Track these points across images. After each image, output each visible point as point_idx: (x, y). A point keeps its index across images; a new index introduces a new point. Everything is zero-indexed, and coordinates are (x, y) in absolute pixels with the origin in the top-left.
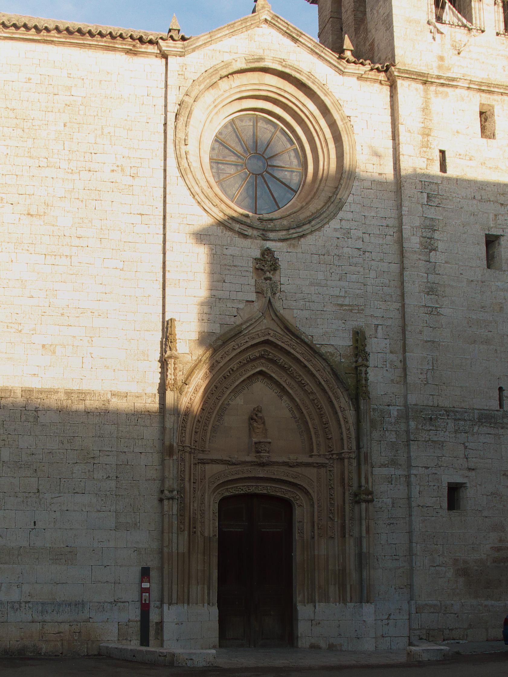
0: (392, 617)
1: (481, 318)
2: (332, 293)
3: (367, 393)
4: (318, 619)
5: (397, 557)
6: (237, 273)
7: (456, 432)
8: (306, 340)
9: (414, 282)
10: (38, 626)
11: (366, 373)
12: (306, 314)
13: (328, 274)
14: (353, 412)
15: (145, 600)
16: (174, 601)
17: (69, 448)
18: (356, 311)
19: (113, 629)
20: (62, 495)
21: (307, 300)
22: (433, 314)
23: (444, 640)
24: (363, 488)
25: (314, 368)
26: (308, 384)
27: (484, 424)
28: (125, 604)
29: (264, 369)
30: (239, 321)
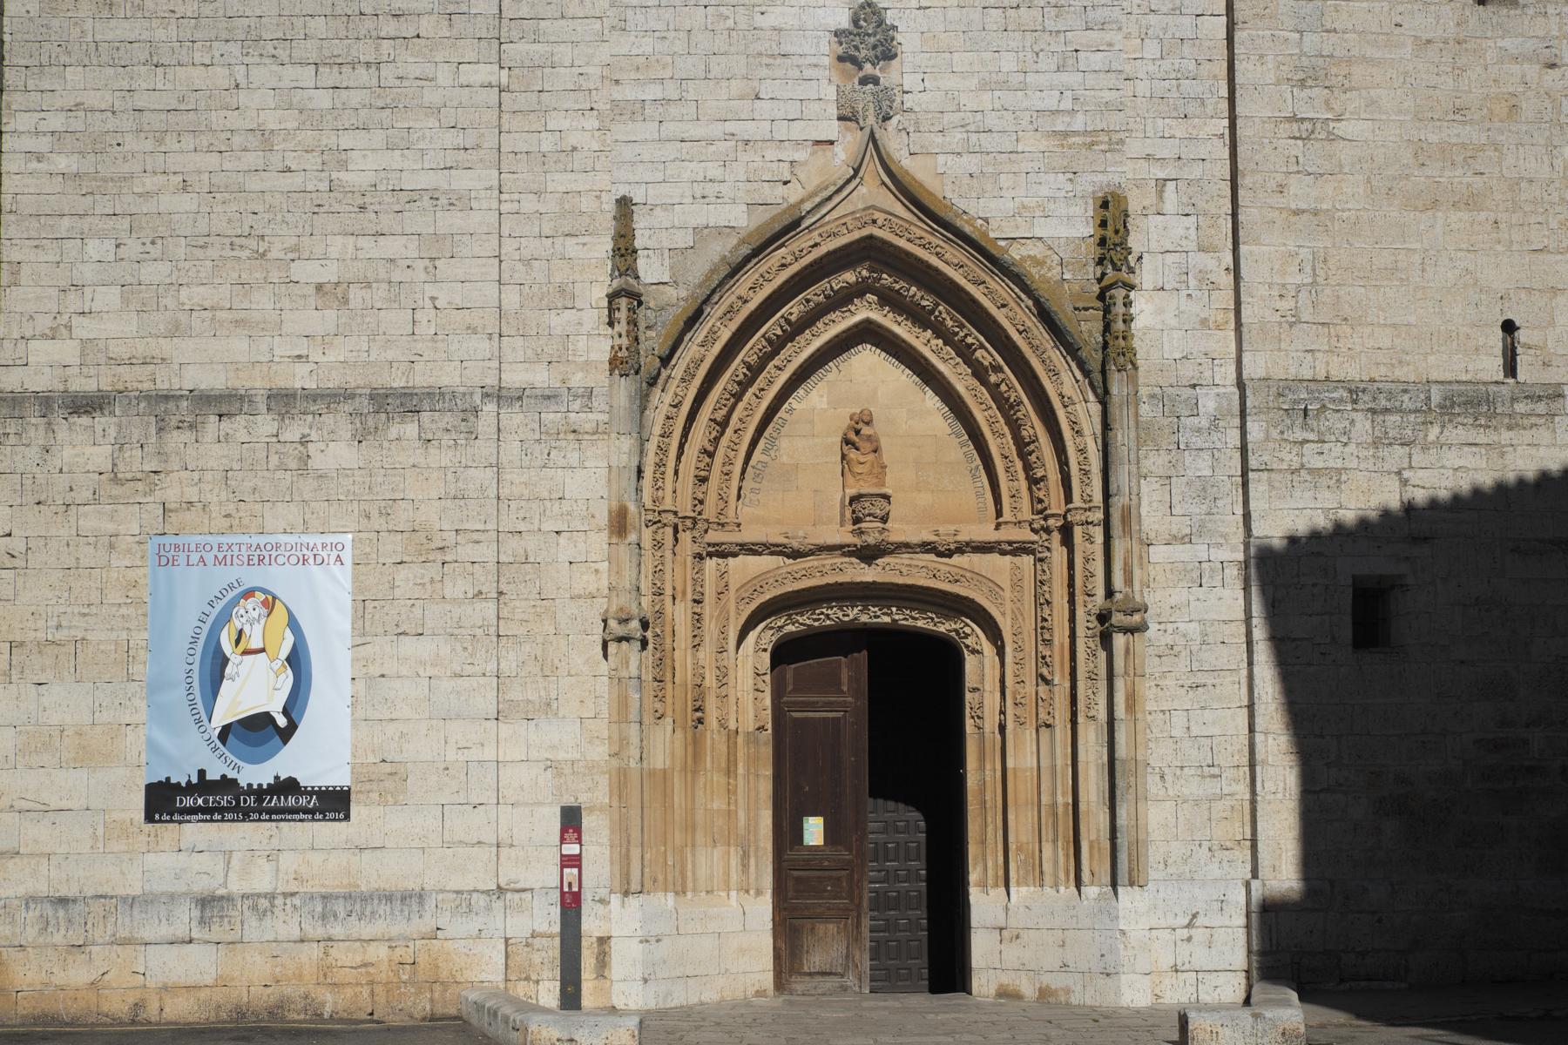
0: (1199, 921)
1: (1454, 140)
2: (1041, 106)
3: (1129, 354)
4: (1016, 924)
5: (1215, 771)
6: (791, 74)
7: (1375, 444)
8: (967, 229)
9: (1261, 56)
10: (313, 952)
11: (1128, 304)
12: (970, 163)
13: (1029, 55)
14: (1095, 408)
15: (570, 885)
16: (635, 886)
17: (384, 527)
18: (1103, 147)
19: (487, 955)
20: (369, 639)
21: (972, 128)
22: (1317, 139)
23: (1342, 980)
24: (1118, 596)
25: (993, 301)
26: (982, 346)
27: (1460, 419)
28: (524, 895)
29: (876, 316)
30: (794, 194)
